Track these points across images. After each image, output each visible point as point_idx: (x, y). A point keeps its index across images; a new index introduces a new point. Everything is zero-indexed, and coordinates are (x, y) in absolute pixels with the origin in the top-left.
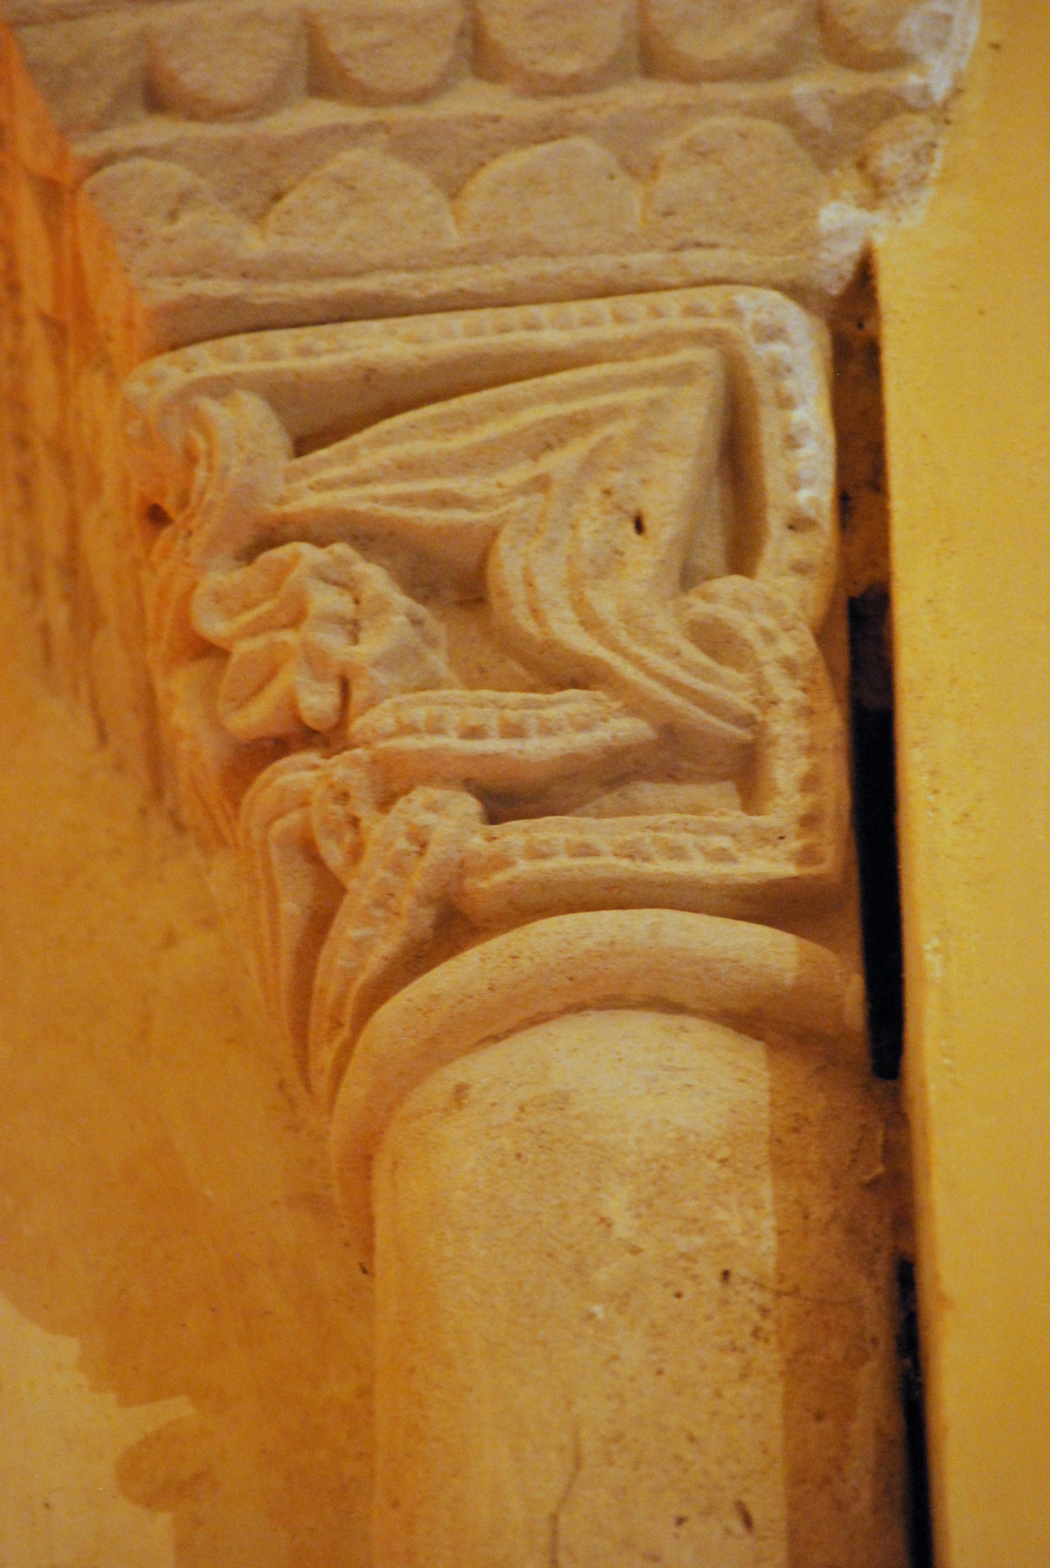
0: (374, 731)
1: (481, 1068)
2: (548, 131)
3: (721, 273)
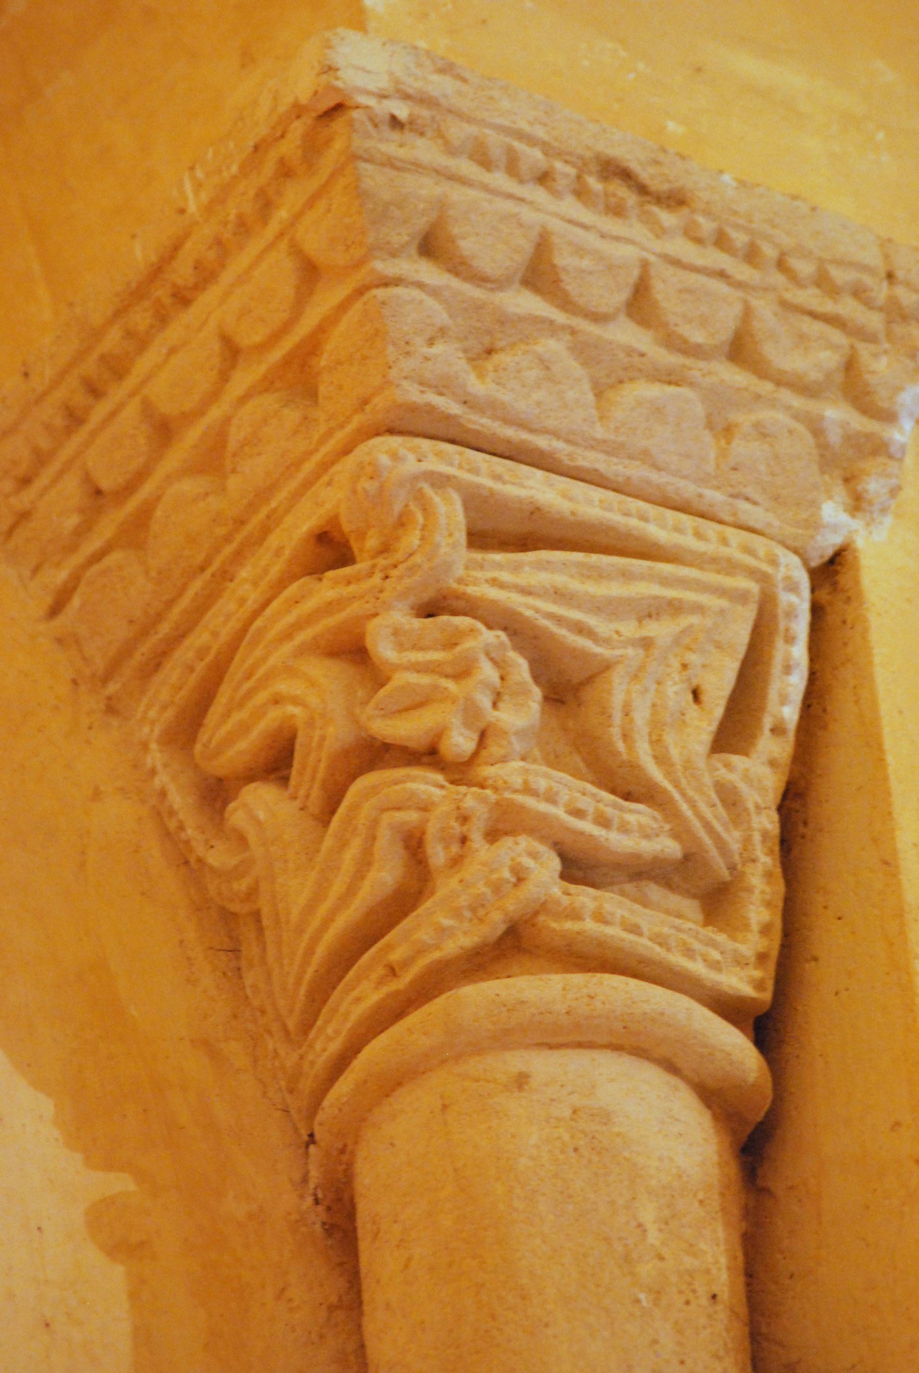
0: (505, 783)
1: (542, 1065)
2: (671, 378)
3: (758, 526)
